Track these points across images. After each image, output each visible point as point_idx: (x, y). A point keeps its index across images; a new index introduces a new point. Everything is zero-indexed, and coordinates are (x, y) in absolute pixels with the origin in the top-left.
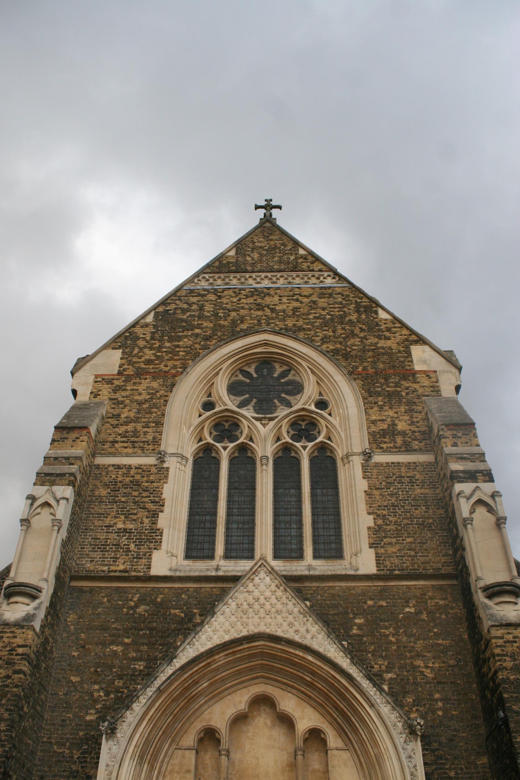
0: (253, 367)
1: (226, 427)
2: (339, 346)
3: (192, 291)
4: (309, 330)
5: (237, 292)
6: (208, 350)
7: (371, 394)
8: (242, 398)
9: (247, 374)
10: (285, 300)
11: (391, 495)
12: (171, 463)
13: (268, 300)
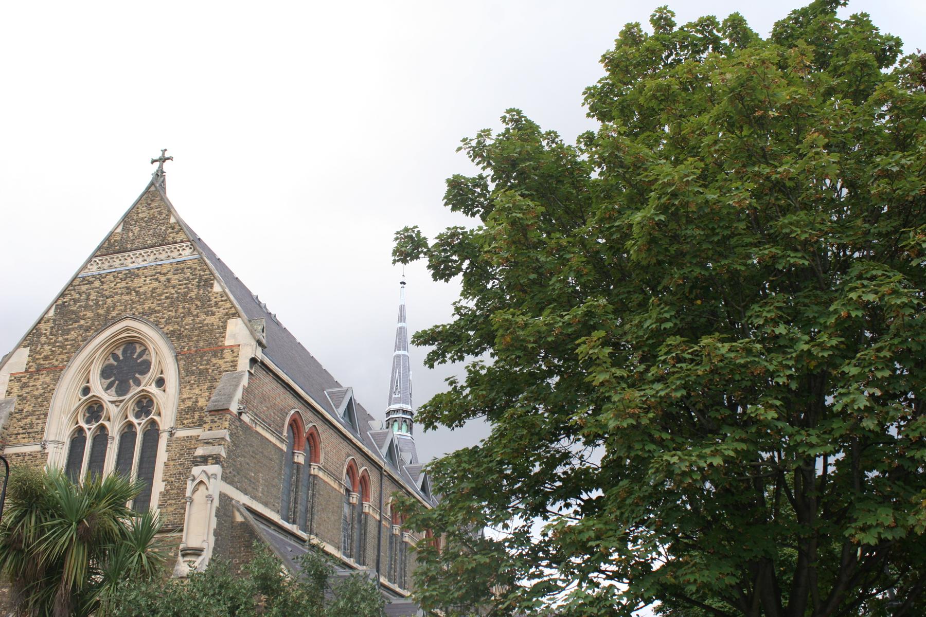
0: (121, 349)
1: (94, 410)
2: (176, 327)
3: (84, 278)
4: (159, 312)
5: (116, 275)
6: (87, 341)
7: (189, 373)
8: (109, 381)
9: (115, 357)
10: (148, 281)
11: (180, 465)
12: (50, 448)
13: (138, 282)
